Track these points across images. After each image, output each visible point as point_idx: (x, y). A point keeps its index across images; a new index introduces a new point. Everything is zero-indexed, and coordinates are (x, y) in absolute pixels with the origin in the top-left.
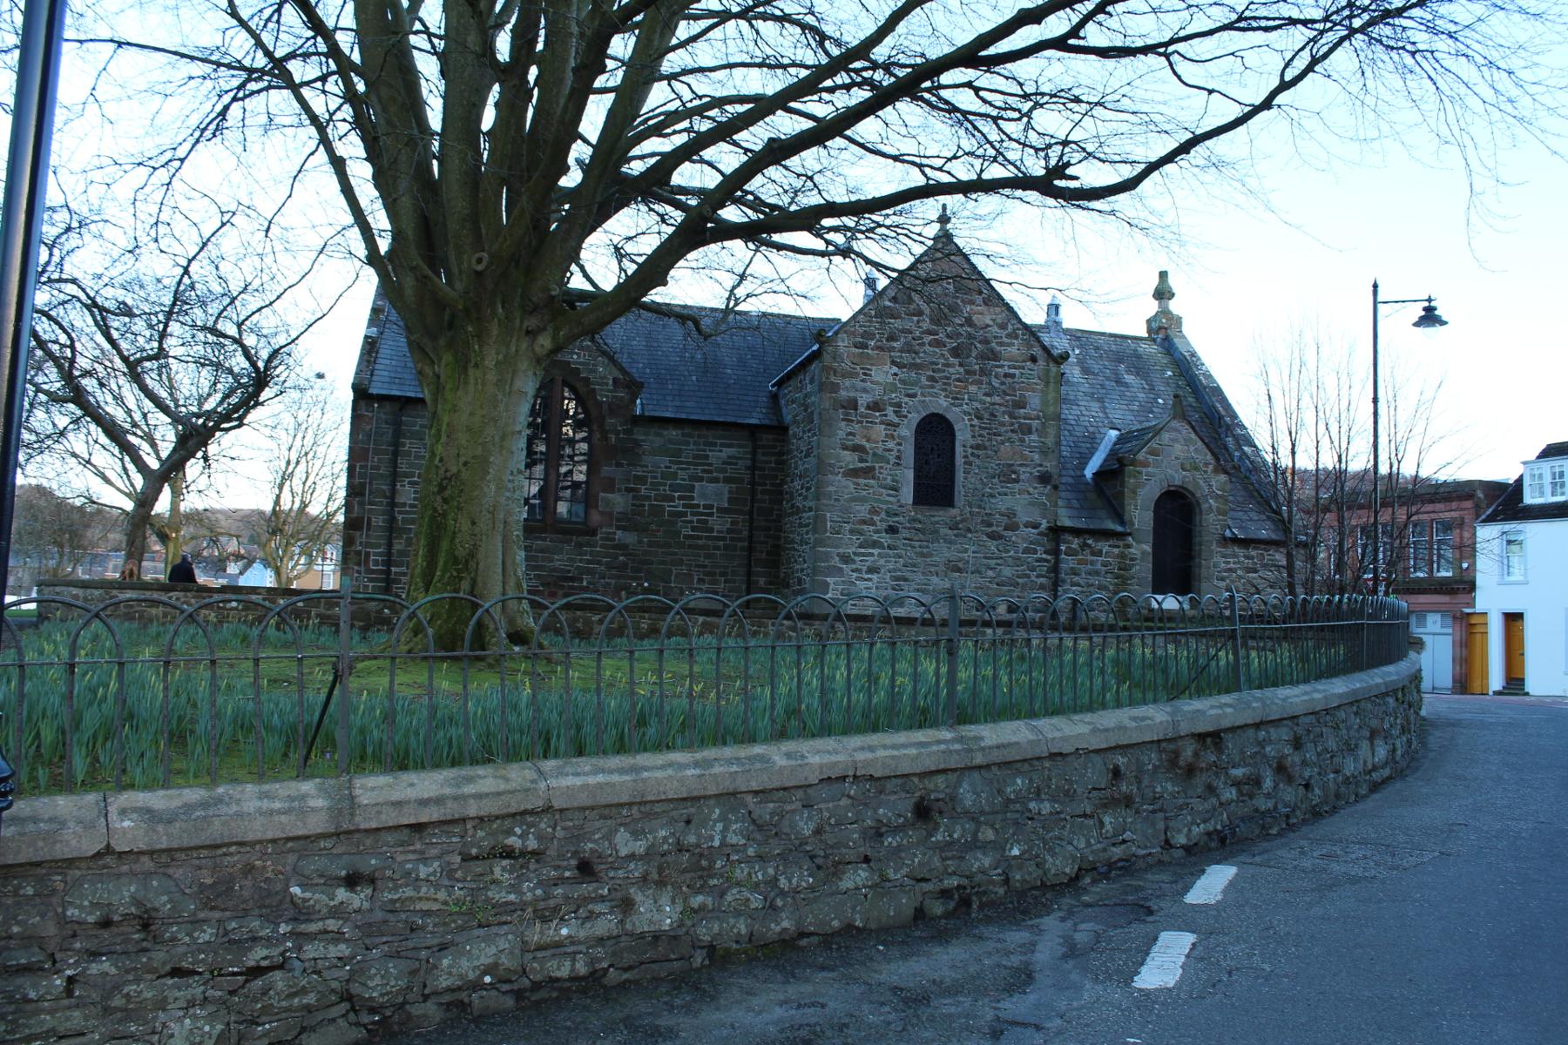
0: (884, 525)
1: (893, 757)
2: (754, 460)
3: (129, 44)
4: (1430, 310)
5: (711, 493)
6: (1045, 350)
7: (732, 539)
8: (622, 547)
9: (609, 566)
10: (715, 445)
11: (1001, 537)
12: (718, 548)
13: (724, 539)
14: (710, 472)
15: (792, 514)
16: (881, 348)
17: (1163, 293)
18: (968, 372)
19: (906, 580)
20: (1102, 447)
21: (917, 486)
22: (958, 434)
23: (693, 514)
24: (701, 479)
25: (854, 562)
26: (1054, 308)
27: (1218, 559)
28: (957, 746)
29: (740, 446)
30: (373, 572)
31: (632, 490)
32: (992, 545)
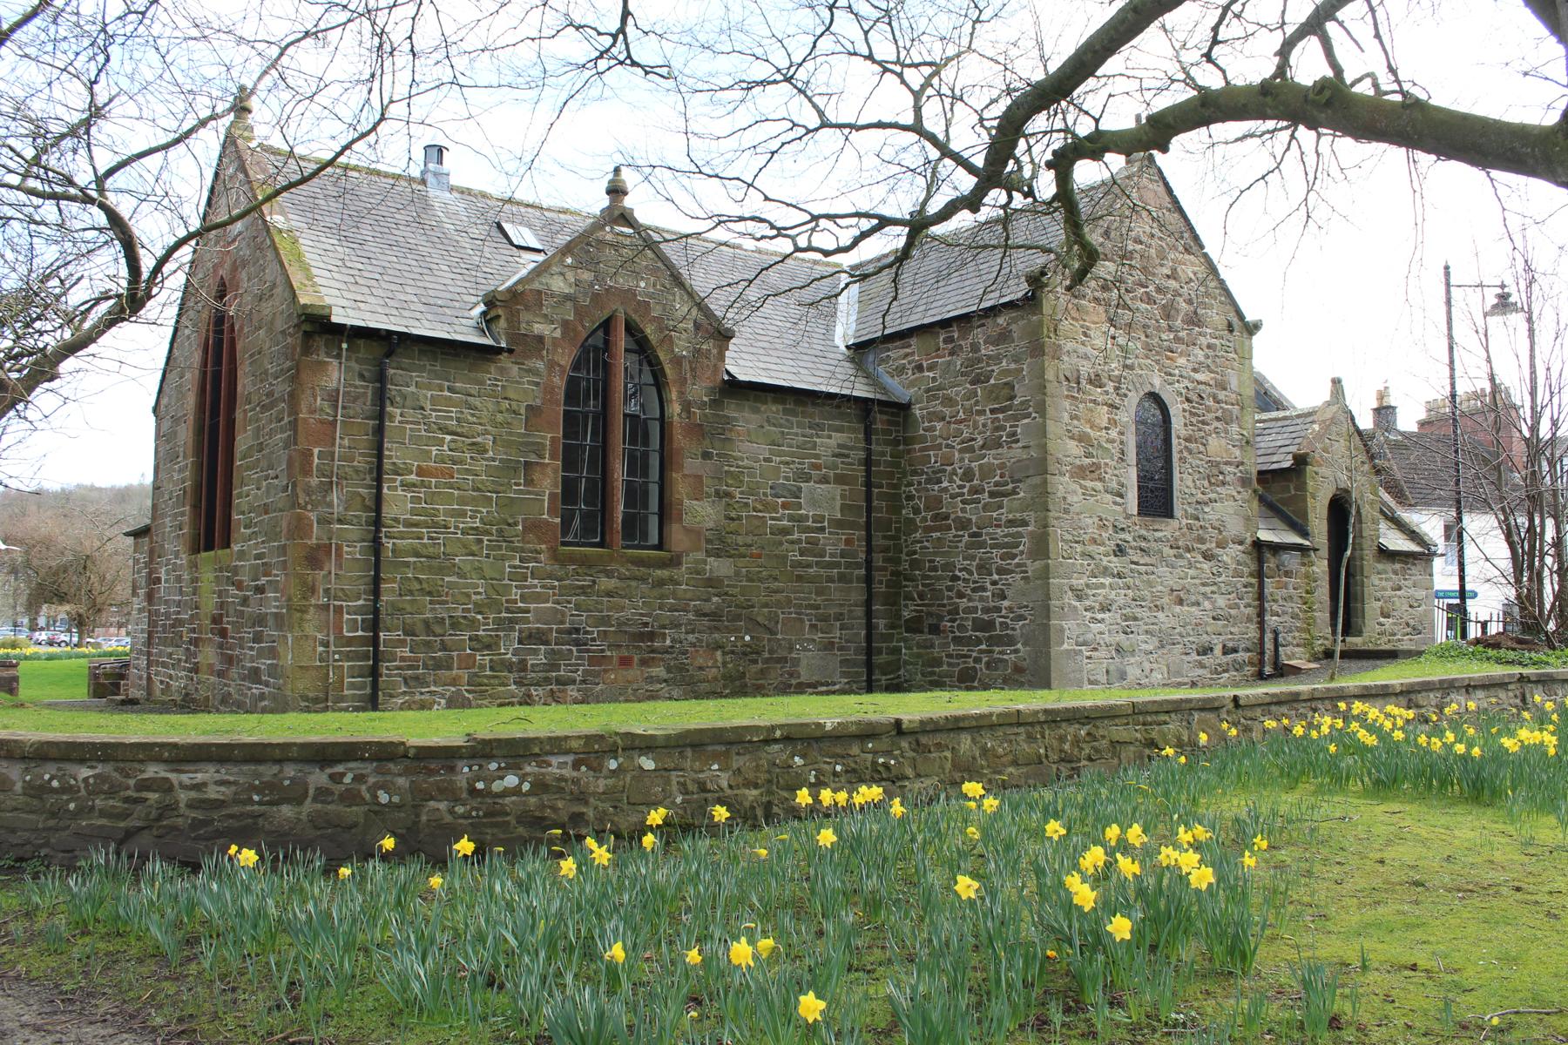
3: (1283, 12)
4: (1503, 297)
5: (824, 500)
7: (848, 565)
8: (712, 582)
10: (820, 427)
13: (838, 565)
19: (1136, 619)
27: (1375, 579)
30: (350, 641)
31: (727, 494)
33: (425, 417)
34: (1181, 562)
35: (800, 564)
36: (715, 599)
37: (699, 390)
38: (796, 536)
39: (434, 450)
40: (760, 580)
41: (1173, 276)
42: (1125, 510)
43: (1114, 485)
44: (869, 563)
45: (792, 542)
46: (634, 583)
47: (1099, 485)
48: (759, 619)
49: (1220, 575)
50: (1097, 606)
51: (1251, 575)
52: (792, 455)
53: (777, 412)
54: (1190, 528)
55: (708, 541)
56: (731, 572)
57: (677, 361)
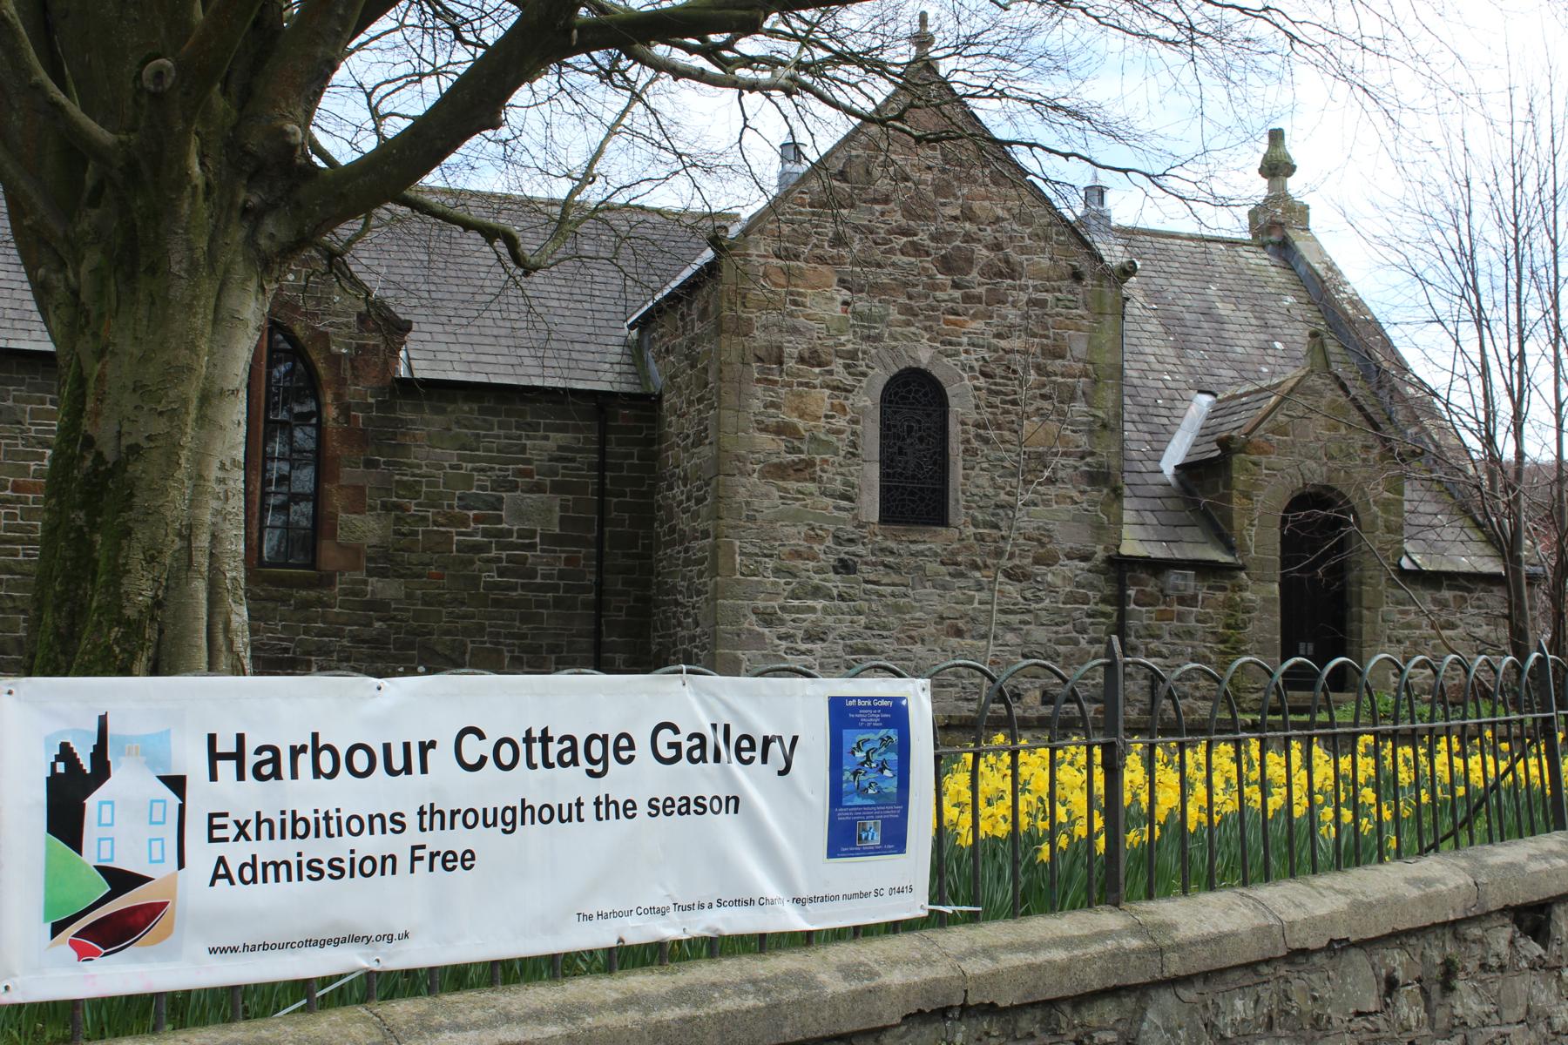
0: (832, 559)
1: (1030, 967)
2: (602, 452)
5: (534, 512)
6: (1086, 264)
7: (568, 589)
8: (378, 606)
9: (355, 639)
10: (534, 427)
11: (1026, 576)
12: (542, 604)
14: (529, 474)
15: (671, 544)
16: (821, 260)
17: (1276, 167)
18: (968, 298)
20: (1185, 424)
21: (886, 492)
22: (952, 402)
23: (501, 547)
24: (514, 487)
25: (782, 622)
26: (1097, 193)
28: (1135, 943)
29: (577, 429)
31: (397, 507)
32: (1012, 589)
33: (22, 431)
34: (961, 583)
35: (496, 586)
36: (377, 625)
37: (361, 390)
38: (493, 554)
39: (33, 465)
40: (441, 604)
41: (968, 215)
42: (855, 517)
43: (838, 485)
44: (600, 587)
45: (488, 561)
46: (270, 605)
47: (811, 487)
48: (438, 648)
49: (1039, 600)
50: (800, 634)
51: (1104, 600)
52: (490, 460)
53: (471, 411)
54: (981, 539)
55: (369, 559)
56: (402, 595)
57: (335, 360)
